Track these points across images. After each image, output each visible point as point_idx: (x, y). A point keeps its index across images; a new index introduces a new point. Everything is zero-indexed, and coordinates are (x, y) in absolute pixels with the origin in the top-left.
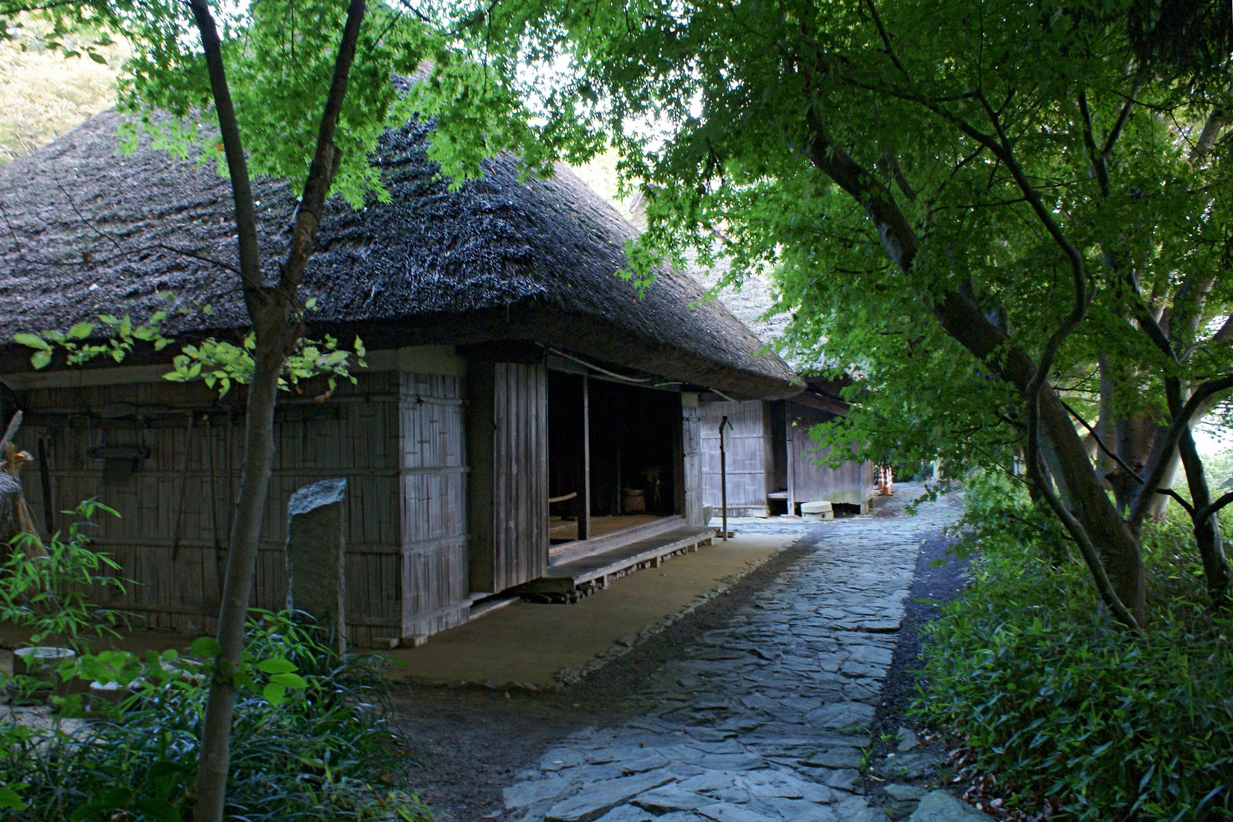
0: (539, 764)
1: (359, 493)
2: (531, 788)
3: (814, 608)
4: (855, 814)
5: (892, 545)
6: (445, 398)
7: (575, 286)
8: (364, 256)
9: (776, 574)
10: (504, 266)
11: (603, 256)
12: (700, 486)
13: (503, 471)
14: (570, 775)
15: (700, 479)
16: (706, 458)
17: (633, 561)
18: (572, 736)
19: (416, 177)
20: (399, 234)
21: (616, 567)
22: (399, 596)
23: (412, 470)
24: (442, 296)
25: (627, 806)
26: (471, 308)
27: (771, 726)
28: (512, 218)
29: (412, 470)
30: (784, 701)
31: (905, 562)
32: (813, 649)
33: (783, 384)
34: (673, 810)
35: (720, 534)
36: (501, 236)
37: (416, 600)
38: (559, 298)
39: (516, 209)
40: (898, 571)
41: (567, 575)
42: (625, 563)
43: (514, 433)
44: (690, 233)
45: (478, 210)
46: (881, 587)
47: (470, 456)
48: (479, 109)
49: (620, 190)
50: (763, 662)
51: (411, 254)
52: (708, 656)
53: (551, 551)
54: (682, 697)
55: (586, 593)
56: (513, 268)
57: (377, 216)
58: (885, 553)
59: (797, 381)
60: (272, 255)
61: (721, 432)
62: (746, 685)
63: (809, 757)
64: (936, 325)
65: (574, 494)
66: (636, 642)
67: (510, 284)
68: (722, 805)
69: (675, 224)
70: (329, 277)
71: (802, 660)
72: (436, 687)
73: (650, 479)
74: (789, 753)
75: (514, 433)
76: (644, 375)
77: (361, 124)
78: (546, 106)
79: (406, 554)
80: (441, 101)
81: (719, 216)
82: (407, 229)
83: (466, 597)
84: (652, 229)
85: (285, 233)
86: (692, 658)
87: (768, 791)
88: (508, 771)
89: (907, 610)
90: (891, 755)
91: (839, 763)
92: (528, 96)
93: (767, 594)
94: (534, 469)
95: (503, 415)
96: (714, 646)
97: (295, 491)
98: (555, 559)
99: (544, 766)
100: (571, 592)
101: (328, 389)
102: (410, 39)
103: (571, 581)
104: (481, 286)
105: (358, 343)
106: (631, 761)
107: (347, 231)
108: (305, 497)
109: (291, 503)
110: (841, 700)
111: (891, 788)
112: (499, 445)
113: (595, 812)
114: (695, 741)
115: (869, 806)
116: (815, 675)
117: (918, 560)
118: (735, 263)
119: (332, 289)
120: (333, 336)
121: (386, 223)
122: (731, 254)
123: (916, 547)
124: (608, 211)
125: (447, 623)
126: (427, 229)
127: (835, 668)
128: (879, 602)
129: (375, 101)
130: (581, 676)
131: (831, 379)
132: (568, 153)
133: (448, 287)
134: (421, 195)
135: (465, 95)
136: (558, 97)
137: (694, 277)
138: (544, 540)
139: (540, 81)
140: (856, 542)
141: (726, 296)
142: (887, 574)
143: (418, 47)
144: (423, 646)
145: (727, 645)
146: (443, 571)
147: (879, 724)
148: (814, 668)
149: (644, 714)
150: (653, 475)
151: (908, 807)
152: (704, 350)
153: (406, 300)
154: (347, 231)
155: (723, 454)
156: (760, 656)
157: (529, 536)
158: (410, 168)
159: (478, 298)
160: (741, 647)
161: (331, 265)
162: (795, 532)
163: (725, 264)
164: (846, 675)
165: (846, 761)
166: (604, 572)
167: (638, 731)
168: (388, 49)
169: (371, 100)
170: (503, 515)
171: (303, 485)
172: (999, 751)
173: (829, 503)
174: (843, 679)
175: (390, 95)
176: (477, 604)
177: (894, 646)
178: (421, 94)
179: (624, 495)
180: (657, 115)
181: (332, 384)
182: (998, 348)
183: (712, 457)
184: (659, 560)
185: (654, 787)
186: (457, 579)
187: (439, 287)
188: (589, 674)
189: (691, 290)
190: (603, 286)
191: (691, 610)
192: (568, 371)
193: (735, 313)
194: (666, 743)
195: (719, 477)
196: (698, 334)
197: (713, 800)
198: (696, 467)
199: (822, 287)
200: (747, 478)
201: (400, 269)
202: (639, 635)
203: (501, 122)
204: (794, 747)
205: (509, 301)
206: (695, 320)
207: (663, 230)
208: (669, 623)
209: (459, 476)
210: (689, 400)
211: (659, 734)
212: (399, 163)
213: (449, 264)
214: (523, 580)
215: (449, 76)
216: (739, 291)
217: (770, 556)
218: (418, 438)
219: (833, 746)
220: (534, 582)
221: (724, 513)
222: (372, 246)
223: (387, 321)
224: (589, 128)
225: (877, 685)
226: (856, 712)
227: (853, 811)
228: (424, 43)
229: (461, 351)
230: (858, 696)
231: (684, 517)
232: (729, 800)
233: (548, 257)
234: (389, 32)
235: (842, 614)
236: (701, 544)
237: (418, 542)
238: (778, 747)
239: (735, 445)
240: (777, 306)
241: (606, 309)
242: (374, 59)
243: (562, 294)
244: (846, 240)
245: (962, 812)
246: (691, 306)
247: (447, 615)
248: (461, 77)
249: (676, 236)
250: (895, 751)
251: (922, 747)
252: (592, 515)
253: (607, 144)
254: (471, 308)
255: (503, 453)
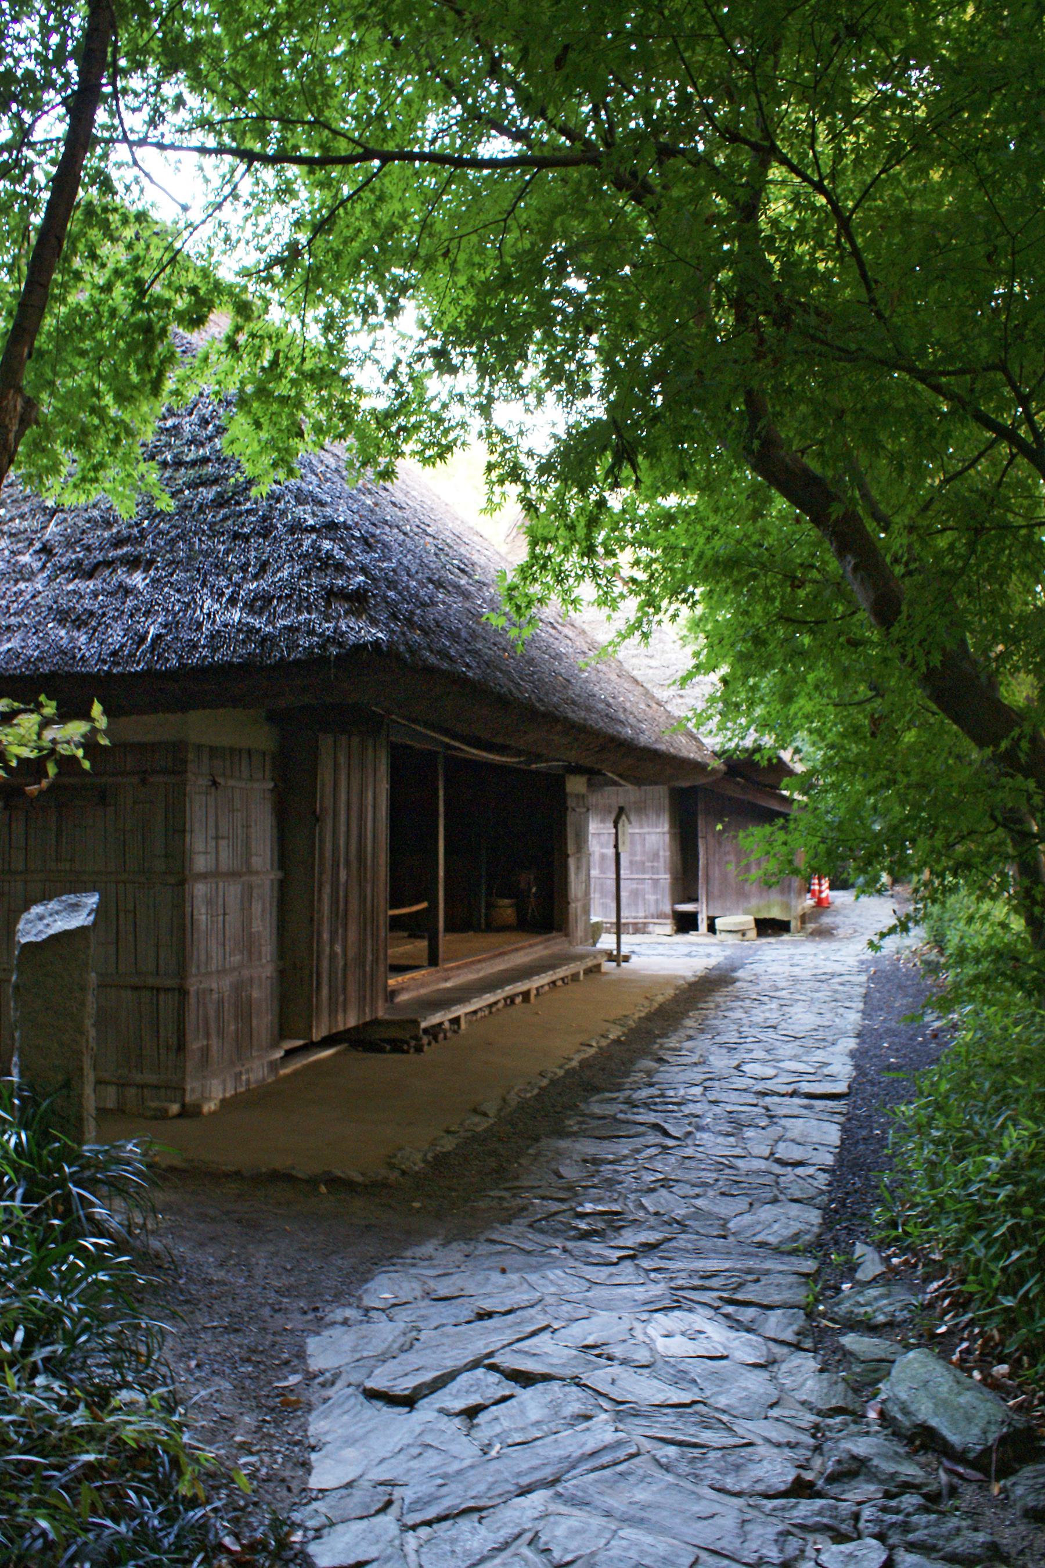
0: (360, 1298)
1: (130, 907)
2: (346, 1338)
3: (735, 1063)
4: (802, 1385)
5: (833, 975)
6: (251, 778)
7: (426, 634)
8: (141, 586)
9: (685, 1014)
10: (328, 604)
11: (466, 595)
12: (587, 893)
13: (327, 877)
14: (403, 1317)
15: (588, 886)
16: (595, 858)
17: (500, 995)
18: (409, 1253)
19: (216, 482)
20: (189, 558)
21: (475, 1004)
22: (181, 1047)
23: (204, 876)
24: (244, 641)
25: (480, 1372)
26: (282, 658)
27: (683, 1241)
28: (342, 539)
29: (204, 876)
30: (699, 1202)
31: (850, 998)
32: (737, 1125)
33: (698, 767)
34: (546, 1378)
35: (610, 957)
36: (327, 563)
37: (206, 1051)
38: (402, 648)
39: (348, 528)
40: (841, 1010)
41: (412, 1016)
42: (489, 998)
43: (343, 828)
44: (585, 561)
45: (297, 527)
46: (820, 1035)
47: (283, 859)
48: (293, 382)
49: (490, 500)
50: (671, 1143)
51: (204, 585)
52: (597, 1133)
53: (391, 982)
54: (561, 1195)
55: (436, 1039)
56: (340, 607)
57: (161, 532)
58: (824, 986)
59: (716, 764)
60: (17, 581)
61: (616, 827)
62: (648, 1177)
63: (735, 1290)
64: (918, 696)
65: (424, 905)
66: (500, 1110)
67: (336, 628)
68: (616, 1370)
69: (566, 551)
70: (92, 614)
71: (721, 1140)
72: (227, 1175)
73: (523, 885)
74: (707, 1283)
75: (343, 828)
76: (519, 753)
77: (131, 399)
78: (386, 381)
79: (192, 989)
80: (243, 369)
81: (622, 543)
82: (201, 551)
83: (275, 1045)
84: (534, 556)
85: (36, 552)
86: (575, 1134)
87: (678, 1346)
88: (316, 1309)
89: (857, 1067)
90: (845, 1286)
91: (776, 1298)
92: (361, 366)
93: (672, 1042)
94: (369, 875)
95: (328, 802)
96: (603, 1118)
97: (27, 909)
98: (394, 993)
99: (367, 1302)
100: (416, 1038)
101: (46, 776)
102: (197, 281)
103: (416, 1023)
104: (297, 629)
105: (97, 709)
106: (489, 1295)
107: (120, 552)
108: (41, 918)
109: (20, 926)
110: (775, 1201)
111: (850, 1341)
112: (322, 841)
113: (436, 1379)
114: (577, 1264)
115: (822, 1371)
116: (739, 1163)
117: (866, 996)
118: (641, 608)
119: (95, 630)
120: (50, 698)
121: (173, 542)
122: (637, 594)
123: (863, 978)
124: (476, 538)
125: (248, 1080)
126: (227, 552)
127: (767, 1153)
128: (820, 1056)
129: (149, 368)
130: (425, 1161)
131: (764, 763)
132: (419, 447)
133: (252, 630)
134: (221, 506)
135: (274, 363)
136: (403, 369)
137: (586, 627)
138: (382, 969)
139: (378, 345)
140: (786, 969)
141: (631, 652)
142: (829, 1016)
143: (209, 292)
144: (212, 1114)
145: (620, 1116)
146: (244, 1011)
147: (828, 1237)
148: (738, 1151)
149: (507, 1222)
150: (528, 881)
151: (875, 1371)
152: (595, 721)
153: (195, 647)
154: (120, 552)
155: (618, 855)
156: (666, 1134)
157: (362, 965)
158: (209, 469)
159: (293, 646)
160: (640, 1118)
161: (96, 596)
162: (709, 955)
163: (630, 606)
164: (780, 1162)
165: (786, 1296)
166: (460, 1011)
167: (500, 1248)
168: (168, 294)
169: (144, 366)
170: (326, 936)
171: (36, 902)
172: (1009, 1302)
173: (750, 918)
174: (777, 1169)
175: (169, 359)
176: (290, 1053)
177: (842, 1119)
178: (213, 357)
179: (489, 906)
180: (540, 400)
181: (52, 769)
182: (1016, 732)
183: (603, 857)
184: (534, 992)
185: (519, 1340)
186: (264, 1022)
187: (239, 631)
188: (435, 1157)
189: (581, 644)
190: (464, 634)
191: (574, 1064)
192: (418, 746)
193: (635, 673)
194: (536, 1268)
195: (613, 883)
196: (587, 702)
197: (603, 1361)
198: (583, 877)
199: (758, 641)
200: (648, 886)
201: (188, 605)
202: (504, 1100)
203: (324, 403)
204: (714, 1275)
205: (334, 651)
206: (586, 681)
207: (549, 557)
208: (544, 1082)
209: (268, 883)
210: (576, 785)
211: (529, 1253)
212: (194, 463)
213: (254, 599)
214: (352, 1022)
215: (253, 336)
216: (647, 644)
217: (677, 988)
218: (212, 832)
219: (767, 1272)
220: (366, 1024)
221: (619, 928)
222: (152, 573)
223: (170, 675)
224: (445, 415)
225: (823, 1178)
226: (796, 1219)
227: (800, 1380)
228: (218, 287)
229: (273, 717)
230: (798, 1195)
231: (567, 935)
232: (624, 1362)
233: (391, 593)
234: (168, 270)
235: (771, 1072)
236: (588, 971)
237: (209, 974)
238: (692, 1273)
239: (632, 843)
240: (697, 667)
241: (467, 665)
242: (148, 308)
243: (407, 644)
244: (795, 578)
245: (956, 1388)
246: (581, 662)
247: (248, 1072)
248: (270, 338)
249: (567, 566)
250: (852, 1279)
251: (889, 1277)
252: (450, 928)
253: (472, 438)
254: (282, 658)
255: (328, 854)
